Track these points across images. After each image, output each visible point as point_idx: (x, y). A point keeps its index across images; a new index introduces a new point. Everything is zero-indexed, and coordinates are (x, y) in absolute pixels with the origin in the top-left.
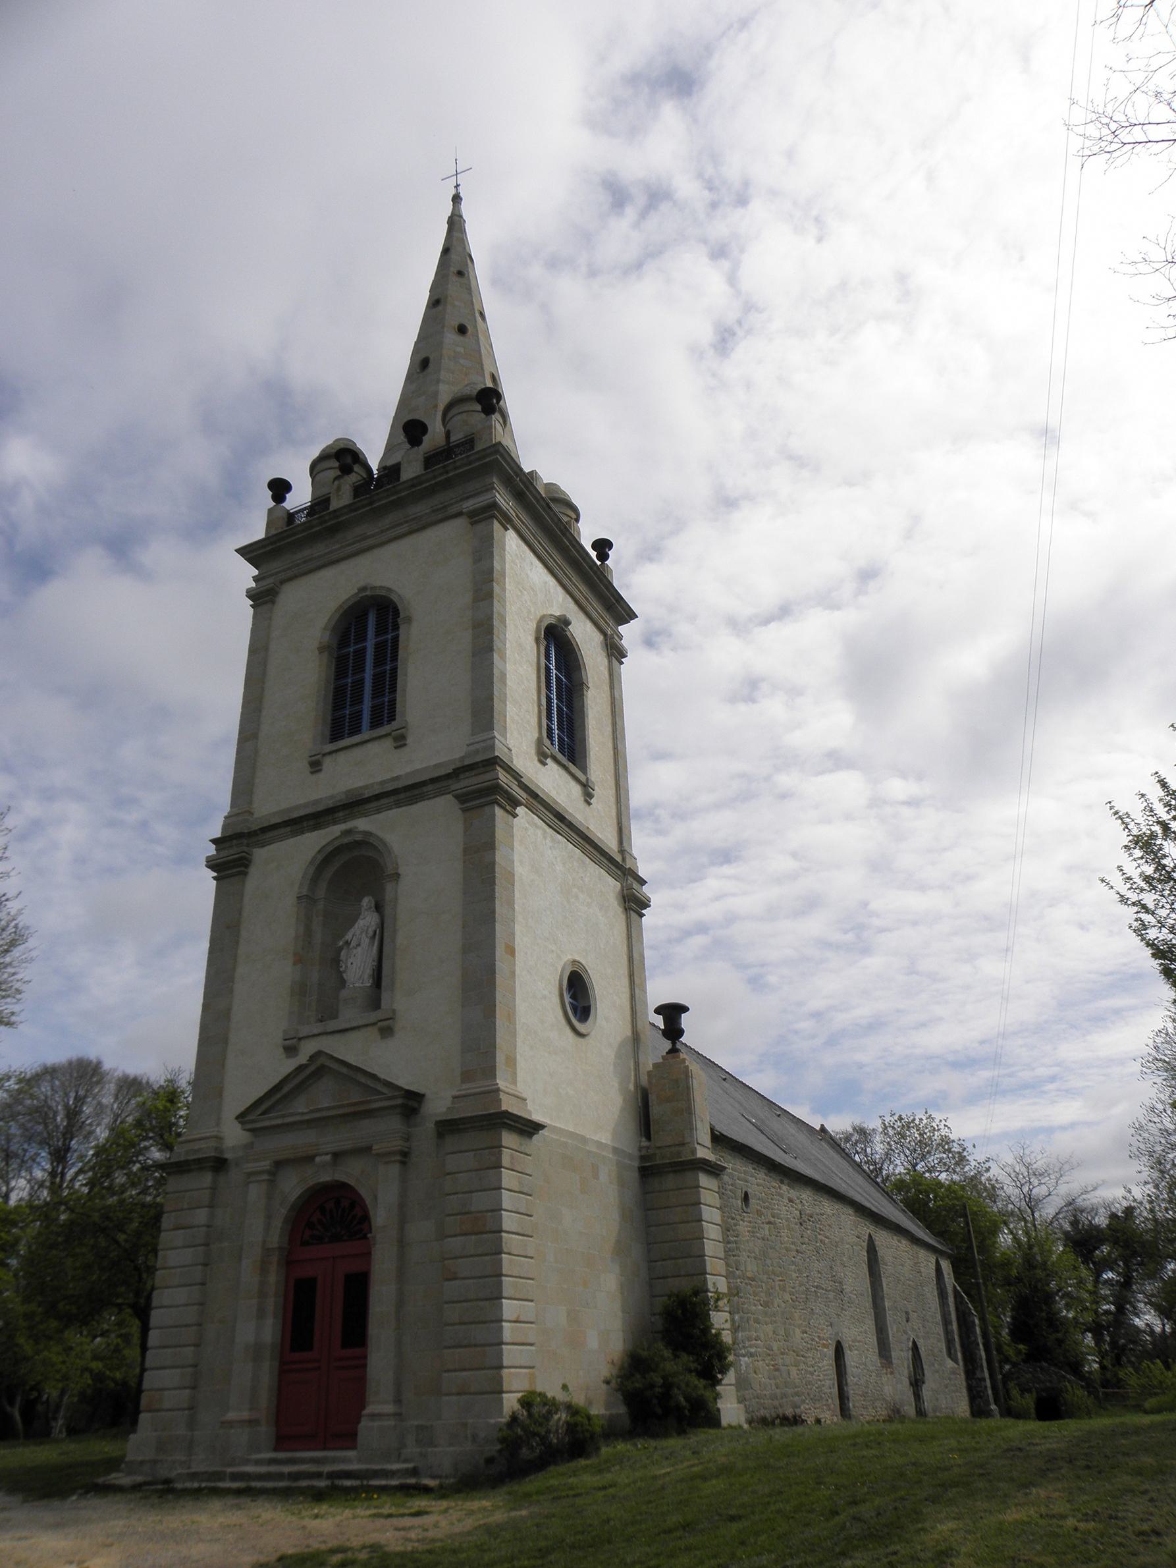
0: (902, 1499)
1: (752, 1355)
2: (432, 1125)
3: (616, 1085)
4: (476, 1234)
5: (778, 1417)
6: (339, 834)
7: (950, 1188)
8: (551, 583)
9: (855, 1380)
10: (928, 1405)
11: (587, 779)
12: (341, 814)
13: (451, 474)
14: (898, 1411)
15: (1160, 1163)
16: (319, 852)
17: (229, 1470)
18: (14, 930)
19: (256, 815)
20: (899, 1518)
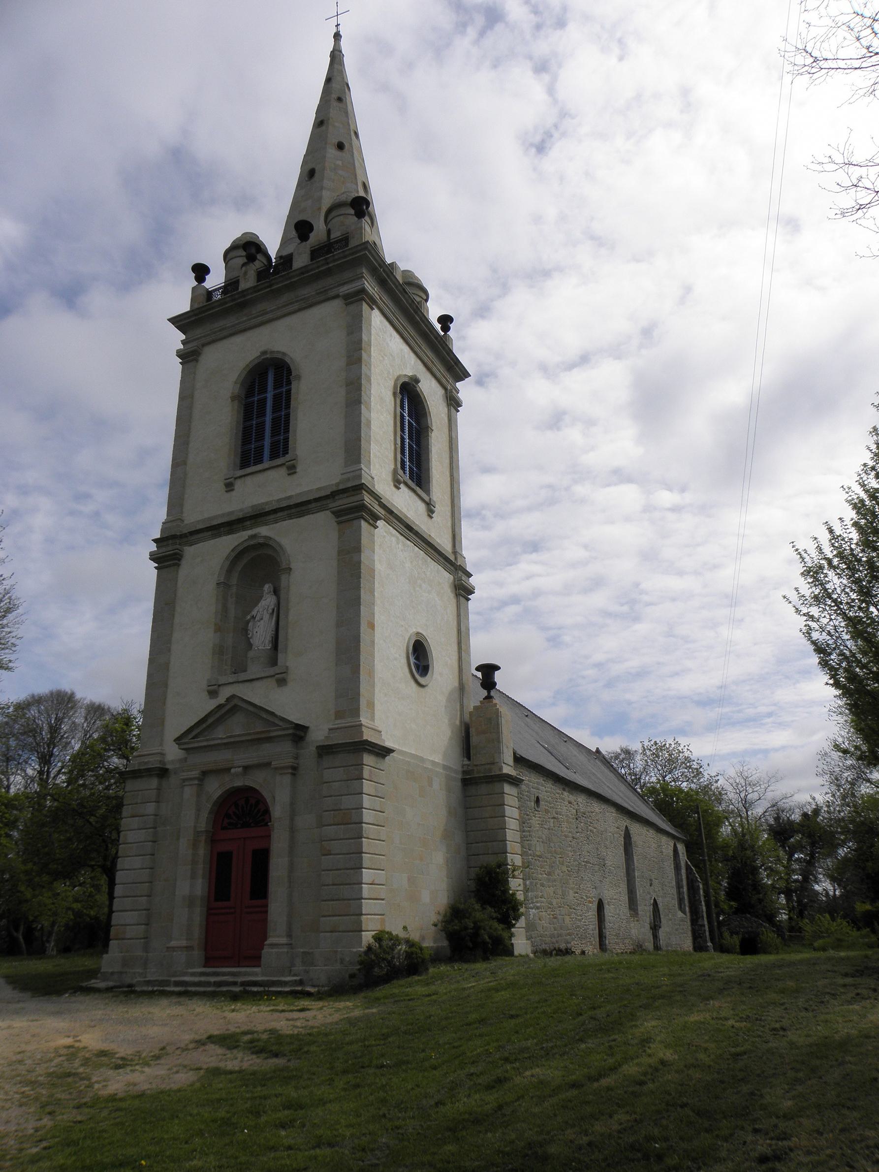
0: (625, 1006)
1: (538, 908)
2: (314, 749)
3: (447, 721)
4: (344, 824)
5: (555, 949)
6: (247, 537)
7: (689, 795)
8: (406, 350)
9: (611, 925)
10: (662, 943)
11: (430, 499)
12: (248, 523)
13: (331, 265)
14: (641, 946)
15: (837, 779)
16: (232, 550)
17: (173, 979)
18: (9, 601)
19: (186, 522)
20: (620, 1018)
